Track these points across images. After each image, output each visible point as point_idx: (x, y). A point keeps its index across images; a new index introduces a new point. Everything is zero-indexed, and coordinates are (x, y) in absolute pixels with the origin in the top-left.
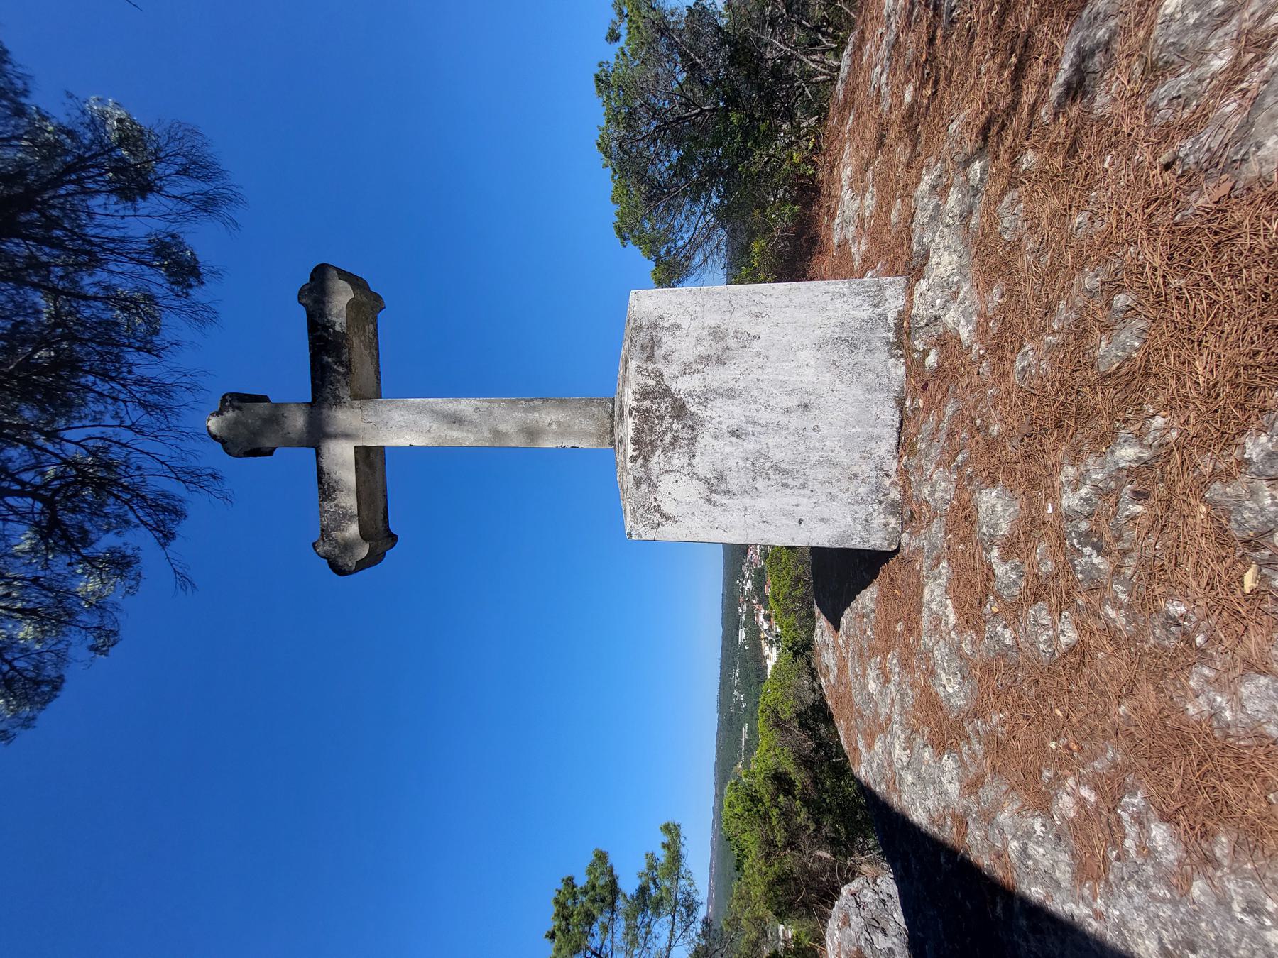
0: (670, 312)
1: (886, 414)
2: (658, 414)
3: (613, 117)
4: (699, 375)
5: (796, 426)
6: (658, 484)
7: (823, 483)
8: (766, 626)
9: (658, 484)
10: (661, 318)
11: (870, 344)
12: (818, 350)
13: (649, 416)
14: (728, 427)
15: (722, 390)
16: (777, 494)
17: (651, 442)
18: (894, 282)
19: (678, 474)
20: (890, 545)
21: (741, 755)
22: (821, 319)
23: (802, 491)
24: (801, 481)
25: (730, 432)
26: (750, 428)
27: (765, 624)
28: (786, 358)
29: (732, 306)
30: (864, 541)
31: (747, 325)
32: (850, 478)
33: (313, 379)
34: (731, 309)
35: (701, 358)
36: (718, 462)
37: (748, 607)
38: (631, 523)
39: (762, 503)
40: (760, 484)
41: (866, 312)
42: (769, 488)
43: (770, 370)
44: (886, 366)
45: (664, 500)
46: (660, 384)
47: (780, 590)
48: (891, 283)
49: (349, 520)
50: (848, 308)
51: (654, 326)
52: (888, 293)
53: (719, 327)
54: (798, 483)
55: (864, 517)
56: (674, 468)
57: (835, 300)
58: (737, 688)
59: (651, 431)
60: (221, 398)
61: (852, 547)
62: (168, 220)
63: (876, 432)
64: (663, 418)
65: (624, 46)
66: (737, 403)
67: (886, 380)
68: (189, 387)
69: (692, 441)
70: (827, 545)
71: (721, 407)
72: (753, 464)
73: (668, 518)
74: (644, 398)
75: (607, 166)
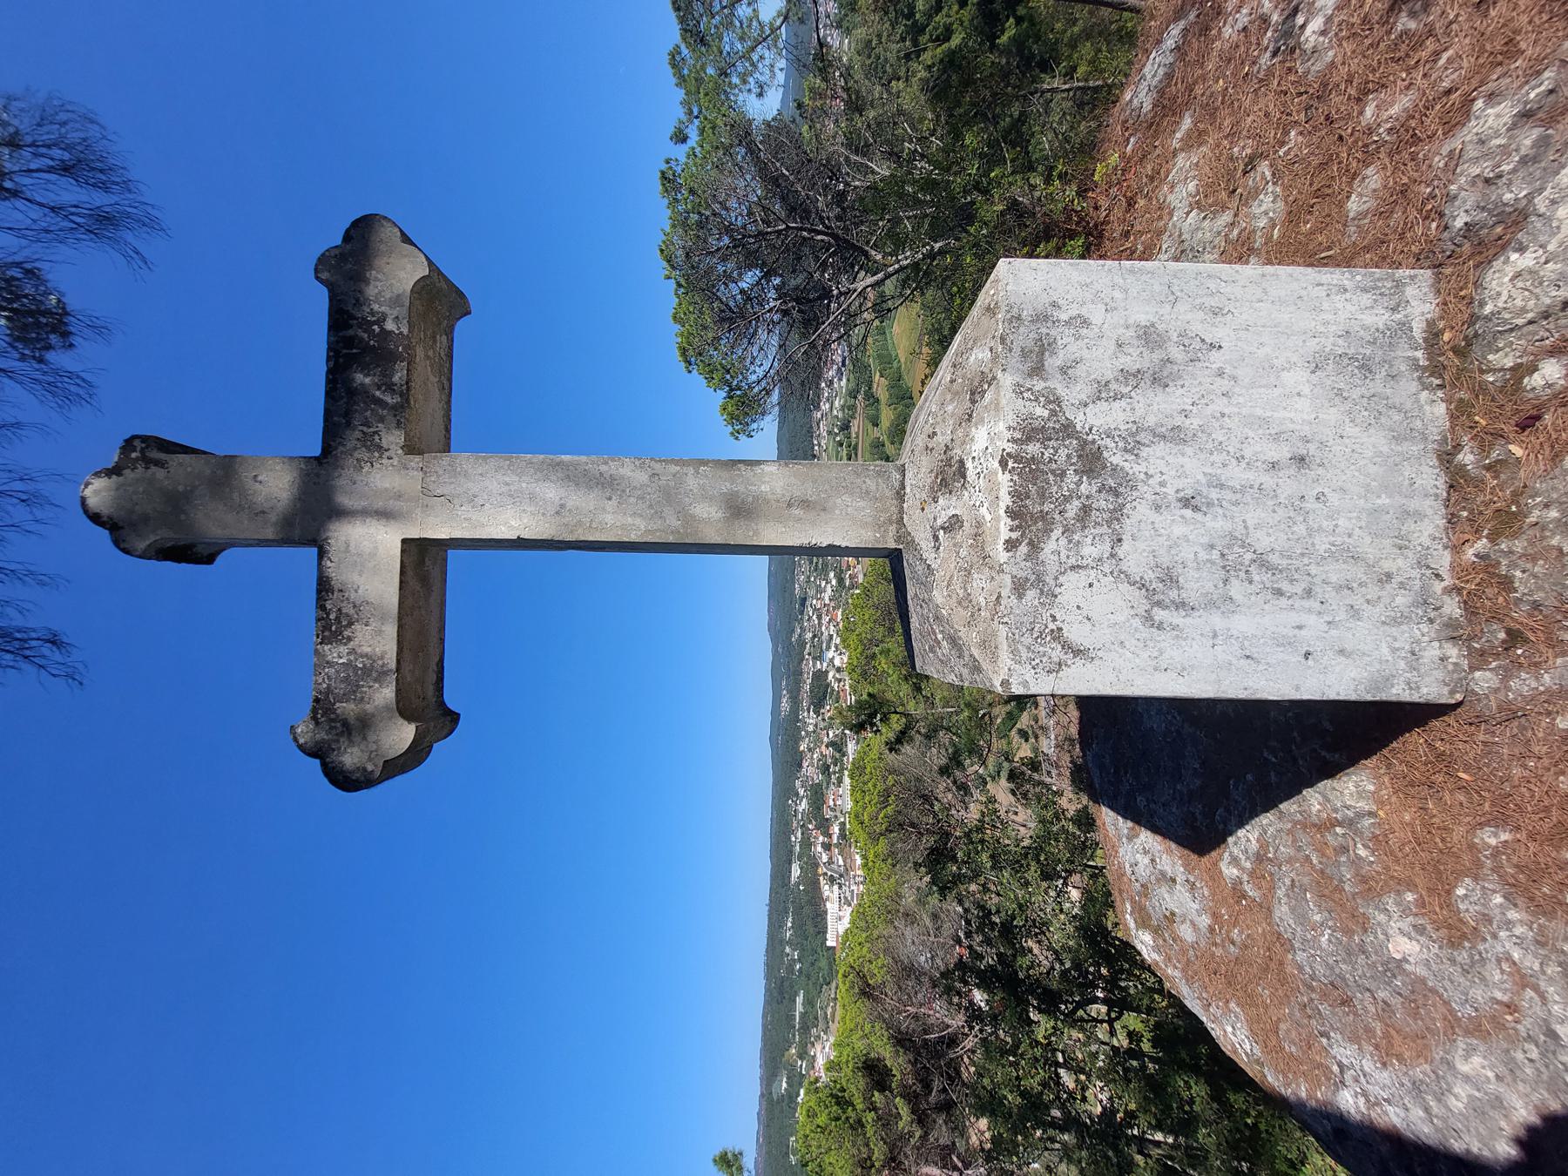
0: (1068, 296)
1: (1425, 476)
2: (1054, 466)
3: (681, 222)
4: (1123, 403)
5: (1290, 492)
6: (1057, 590)
7: (1339, 588)
8: (825, 858)
9: (1057, 590)
10: (1054, 305)
11: (1391, 366)
12: (1313, 372)
13: (1038, 469)
14: (1178, 491)
15: (1163, 430)
16: (1266, 607)
17: (1043, 516)
18: (1416, 276)
19: (1093, 573)
20: (1452, 692)
21: (794, 1035)
22: (1314, 323)
23: (1307, 603)
24: (1303, 586)
25: (1180, 500)
26: (1214, 494)
27: (824, 855)
28: (1265, 382)
29: (1173, 293)
30: (1411, 688)
31: (1198, 325)
32: (1380, 581)
33: (328, 414)
34: (1172, 298)
35: (1125, 375)
36: (1162, 551)
37: (802, 834)
38: (1009, 662)
39: (1242, 624)
40: (1236, 589)
41: (1379, 318)
42: (1253, 598)
43: (1241, 400)
44: (1417, 401)
45: (1068, 619)
46: (1056, 415)
47: (865, 809)
48: (1412, 278)
49: (376, 680)
50: (1353, 309)
51: (1042, 318)
52: (1410, 291)
53: (1153, 325)
54: (1298, 588)
55: (1407, 647)
56: (1085, 562)
57: (1332, 297)
58: (790, 943)
59: (1043, 496)
60: (121, 443)
61: (1394, 699)
62: (24, 237)
63: (1414, 504)
64: (1063, 474)
65: (696, 146)
66: (1189, 450)
67: (1418, 423)
68: (24, 497)
69: (1116, 515)
70: (1353, 697)
71: (1163, 458)
72: (1223, 555)
73: (1078, 652)
74: (1029, 439)
75: (669, 278)
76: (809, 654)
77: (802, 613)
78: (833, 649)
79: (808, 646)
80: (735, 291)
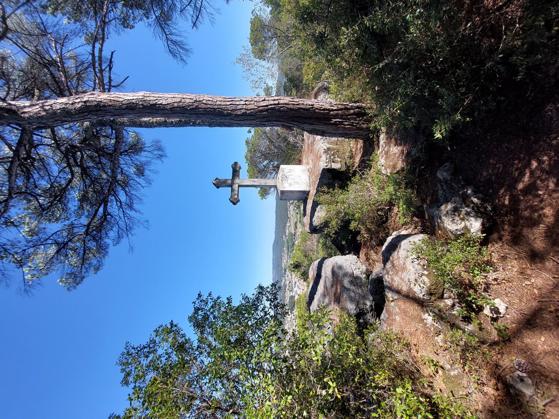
3: (249, 151)
76: (288, 289)
77: (285, 274)
78: (297, 287)
79: (287, 286)
80: (262, 165)
